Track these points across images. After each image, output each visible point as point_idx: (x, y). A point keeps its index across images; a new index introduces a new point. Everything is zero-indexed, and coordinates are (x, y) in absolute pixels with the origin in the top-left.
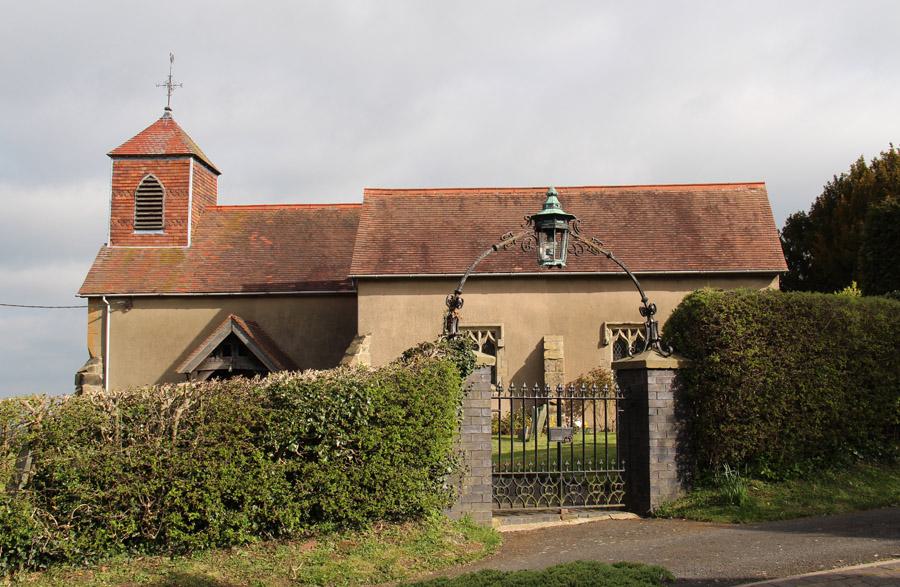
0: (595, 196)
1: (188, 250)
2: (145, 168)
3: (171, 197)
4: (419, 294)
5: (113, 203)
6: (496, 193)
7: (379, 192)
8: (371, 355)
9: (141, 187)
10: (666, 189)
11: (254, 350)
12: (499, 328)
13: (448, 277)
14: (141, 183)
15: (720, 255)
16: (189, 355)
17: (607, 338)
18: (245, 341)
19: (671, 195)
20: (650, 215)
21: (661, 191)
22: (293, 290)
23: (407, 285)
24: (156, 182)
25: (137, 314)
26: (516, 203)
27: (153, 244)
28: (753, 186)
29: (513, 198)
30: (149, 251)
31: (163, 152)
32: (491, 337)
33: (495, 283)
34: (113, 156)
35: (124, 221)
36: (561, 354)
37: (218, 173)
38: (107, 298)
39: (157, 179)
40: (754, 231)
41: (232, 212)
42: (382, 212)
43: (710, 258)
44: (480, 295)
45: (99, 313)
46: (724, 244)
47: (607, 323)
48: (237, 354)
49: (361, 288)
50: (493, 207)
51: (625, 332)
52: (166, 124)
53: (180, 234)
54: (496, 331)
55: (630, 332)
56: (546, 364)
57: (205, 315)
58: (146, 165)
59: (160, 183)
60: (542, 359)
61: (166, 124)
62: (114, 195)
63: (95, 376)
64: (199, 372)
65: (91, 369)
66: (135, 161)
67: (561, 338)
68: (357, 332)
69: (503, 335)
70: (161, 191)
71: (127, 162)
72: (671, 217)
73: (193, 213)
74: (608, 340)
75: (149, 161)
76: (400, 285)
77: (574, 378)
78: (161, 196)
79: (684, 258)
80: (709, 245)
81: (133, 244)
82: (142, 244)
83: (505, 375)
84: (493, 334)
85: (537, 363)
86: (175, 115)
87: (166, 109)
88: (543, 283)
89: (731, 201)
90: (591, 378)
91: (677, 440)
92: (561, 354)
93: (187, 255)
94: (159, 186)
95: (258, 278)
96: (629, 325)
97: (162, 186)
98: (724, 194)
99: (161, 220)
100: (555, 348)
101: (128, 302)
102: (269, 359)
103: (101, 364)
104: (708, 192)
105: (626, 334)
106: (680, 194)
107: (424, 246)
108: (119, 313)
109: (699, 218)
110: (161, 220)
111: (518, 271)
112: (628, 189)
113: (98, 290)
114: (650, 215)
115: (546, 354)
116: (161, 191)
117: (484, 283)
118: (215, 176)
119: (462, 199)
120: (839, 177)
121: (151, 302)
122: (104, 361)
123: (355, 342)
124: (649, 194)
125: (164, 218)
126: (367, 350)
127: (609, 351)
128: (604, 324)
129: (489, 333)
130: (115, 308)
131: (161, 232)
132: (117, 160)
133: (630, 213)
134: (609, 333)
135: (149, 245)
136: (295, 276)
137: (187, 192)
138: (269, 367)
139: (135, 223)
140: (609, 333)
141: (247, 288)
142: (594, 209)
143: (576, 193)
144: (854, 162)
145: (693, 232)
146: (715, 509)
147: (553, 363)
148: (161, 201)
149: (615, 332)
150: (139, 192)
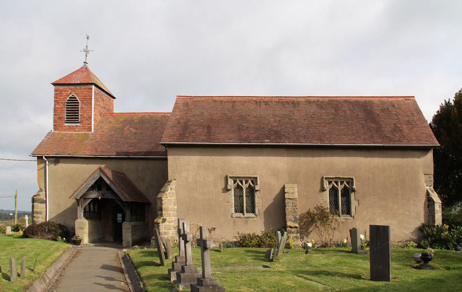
0: (314, 102)
3: (84, 106)
4: (205, 156)
6: (255, 99)
7: (186, 98)
8: (177, 193)
9: (68, 100)
10: (356, 99)
11: (113, 187)
12: (256, 178)
14: (68, 99)
15: (395, 136)
17: (325, 186)
18: (108, 182)
19: (359, 102)
20: (348, 112)
21: (353, 99)
22: (143, 155)
23: (198, 149)
24: (75, 98)
25: (62, 166)
26: (266, 105)
27: (75, 131)
28: (408, 98)
29: (264, 102)
30: (72, 134)
31: (79, 82)
32: (251, 184)
33: (252, 150)
34: (54, 84)
35: (60, 118)
36: (296, 195)
37: (114, 98)
38: (46, 157)
39: (76, 96)
40: (413, 123)
41: (118, 116)
42: (185, 109)
43: (389, 137)
44: (243, 157)
45: (43, 165)
46: (396, 129)
47: (325, 177)
48: (105, 189)
49: (170, 151)
50: (252, 106)
51: (336, 183)
52: (85, 70)
53: (88, 126)
54: (350, 182)
55: (244, 182)
56: (286, 202)
57: (93, 167)
58: (70, 89)
59: (78, 98)
60: (283, 199)
61: (85, 70)
62: (55, 105)
63: (41, 199)
64: (84, 199)
65: (38, 195)
66: (65, 87)
67: (296, 185)
68: (167, 178)
69: (258, 183)
70: (78, 103)
71: (61, 88)
72: (361, 115)
73: (95, 115)
74: (326, 187)
75: (72, 87)
76: (193, 149)
77: (305, 211)
78: (78, 105)
79: (372, 137)
80: (387, 130)
81: (65, 130)
83: (260, 208)
84: (252, 182)
85: (281, 202)
86: (89, 66)
87: (85, 63)
88: (284, 150)
89: (396, 106)
90: (316, 212)
92: (296, 195)
93: (91, 136)
94: (77, 100)
95: (125, 149)
96: (339, 178)
97: (79, 100)
98: (391, 102)
99: (78, 118)
100: (293, 192)
101: (57, 160)
102: (121, 193)
103: (44, 192)
104: (381, 101)
105: (242, 183)
106: (365, 101)
107: (209, 127)
108: (52, 165)
109: (378, 115)
110: (78, 118)
111: (267, 142)
112: (334, 99)
113: (40, 154)
114: (348, 112)
115: (286, 195)
116: (78, 103)
118: (112, 99)
119: (234, 102)
120: (447, 101)
121: (69, 160)
122: (46, 191)
123: (166, 184)
124: (346, 101)
125: (80, 117)
126: (173, 190)
127: (327, 194)
128: (323, 178)
129: (250, 181)
130: (51, 162)
131: (78, 124)
134: (231, 182)
135: (73, 131)
136: (145, 147)
137: (91, 104)
139: (66, 119)
140: (231, 182)
141: (118, 154)
142: (314, 108)
143: (303, 100)
145: (376, 122)
147: (291, 201)
148: (78, 108)
149: (330, 183)
150: (67, 103)
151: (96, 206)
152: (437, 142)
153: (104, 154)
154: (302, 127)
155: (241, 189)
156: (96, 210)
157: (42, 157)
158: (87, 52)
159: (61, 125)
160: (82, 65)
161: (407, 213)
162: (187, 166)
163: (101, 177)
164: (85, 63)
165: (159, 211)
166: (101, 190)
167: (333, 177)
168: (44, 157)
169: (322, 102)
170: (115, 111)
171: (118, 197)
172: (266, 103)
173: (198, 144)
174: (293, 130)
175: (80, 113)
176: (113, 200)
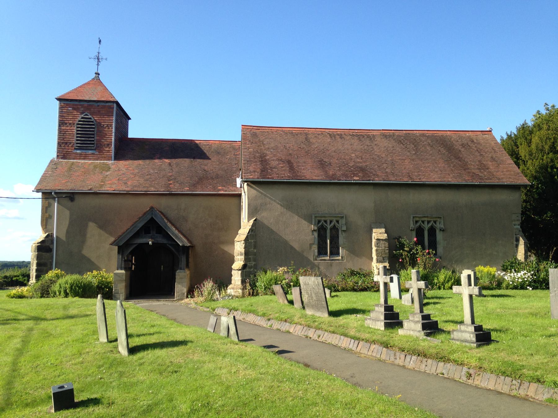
2: (82, 109)
7: (251, 128)
9: (80, 121)
13: (286, 182)
26: (341, 138)
29: (338, 135)
34: (59, 99)
46: (483, 167)
57: (134, 243)
98: (469, 137)
107: (289, 162)
113: (50, 186)
117: (331, 187)
124: (423, 135)
133: (415, 146)
139: (76, 145)
144: (535, 113)
153: (139, 189)
154: (386, 164)
155: (325, 229)
161: (496, 253)
163: (152, 217)
164: (96, 74)
167: (421, 216)
169: (398, 136)
170: (131, 135)
172: (341, 136)
173: (261, 181)
174: (379, 167)
175: (96, 138)
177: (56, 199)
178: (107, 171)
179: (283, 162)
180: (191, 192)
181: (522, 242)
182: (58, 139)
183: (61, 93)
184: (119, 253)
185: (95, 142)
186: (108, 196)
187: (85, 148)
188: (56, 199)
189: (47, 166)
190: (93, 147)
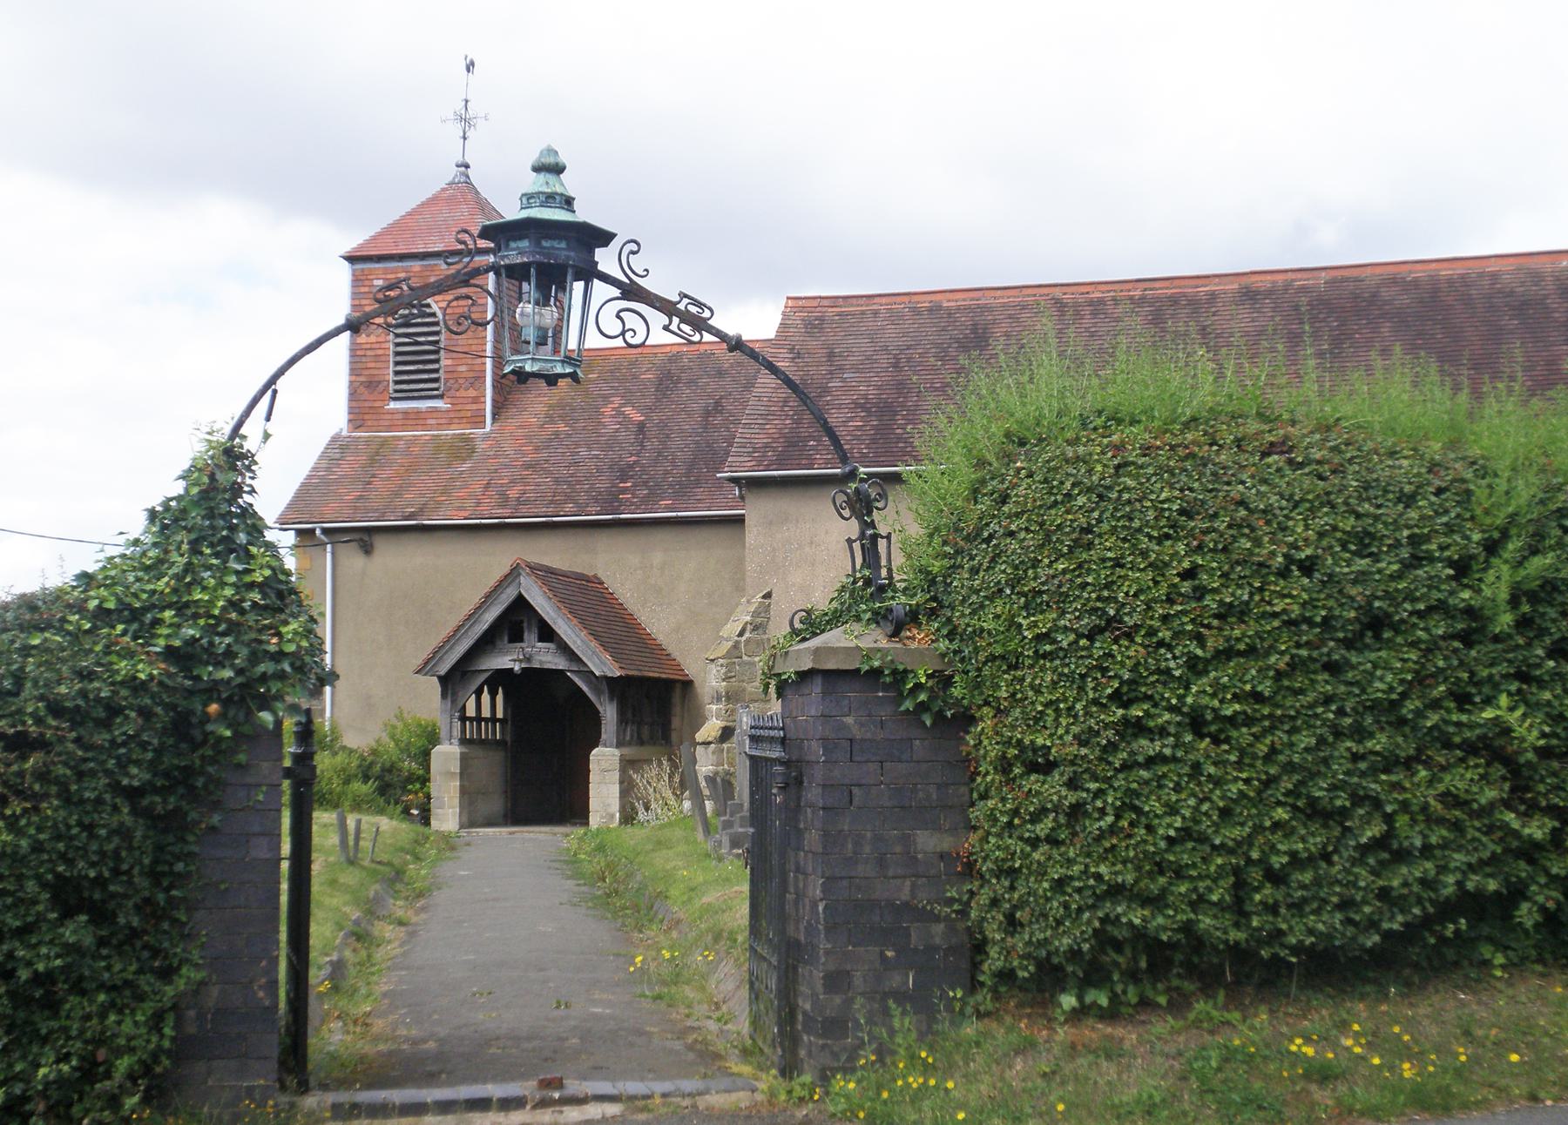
0: (1270, 293)
1: (486, 437)
5: (351, 350)
7: (815, 303)
16: (1209, 981)
25: (392, 558)
27: (425, 427)
29: (1091, 303)
34: (351, 259)
53: (474, 407)
81: (389, 428)
82: (404, 427)
91: (611, 699)
93: (481, 446)
101: (365, 538)
106: (1463, 276)
117: (613, 532)
124: (1394, 281)
132: (359, 266)
138: (558, 1075)
146: (1488, 870)
151: (500, 698)
152: (530, 1083)
156: (500, 715)
157: (313, 531)
158: (465, 120)
159: (377, 411)
160: (451, 173)
162: (807, 549)
163: (520, 593)
165: (712, 703)
166: (521, 640)
168: (318, 532)
171: (579, 660)
175: (443, 362)
176: (562, 672)
177: (329, 547)
178: (464, 460)
179: (868, 410)
180: (674, 514)
181: (500, 690)
182: (351, 375)
183: (353, 240)
184: (444, 695)
185: (441, 374)
186: (453, 534)
187: (416, 394)
188: (329, 547)
189: (319, 453)
190: (437, 389)
